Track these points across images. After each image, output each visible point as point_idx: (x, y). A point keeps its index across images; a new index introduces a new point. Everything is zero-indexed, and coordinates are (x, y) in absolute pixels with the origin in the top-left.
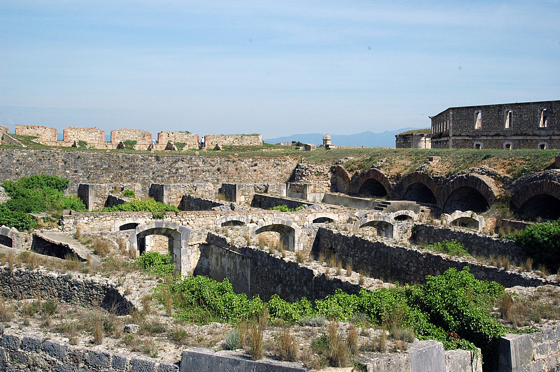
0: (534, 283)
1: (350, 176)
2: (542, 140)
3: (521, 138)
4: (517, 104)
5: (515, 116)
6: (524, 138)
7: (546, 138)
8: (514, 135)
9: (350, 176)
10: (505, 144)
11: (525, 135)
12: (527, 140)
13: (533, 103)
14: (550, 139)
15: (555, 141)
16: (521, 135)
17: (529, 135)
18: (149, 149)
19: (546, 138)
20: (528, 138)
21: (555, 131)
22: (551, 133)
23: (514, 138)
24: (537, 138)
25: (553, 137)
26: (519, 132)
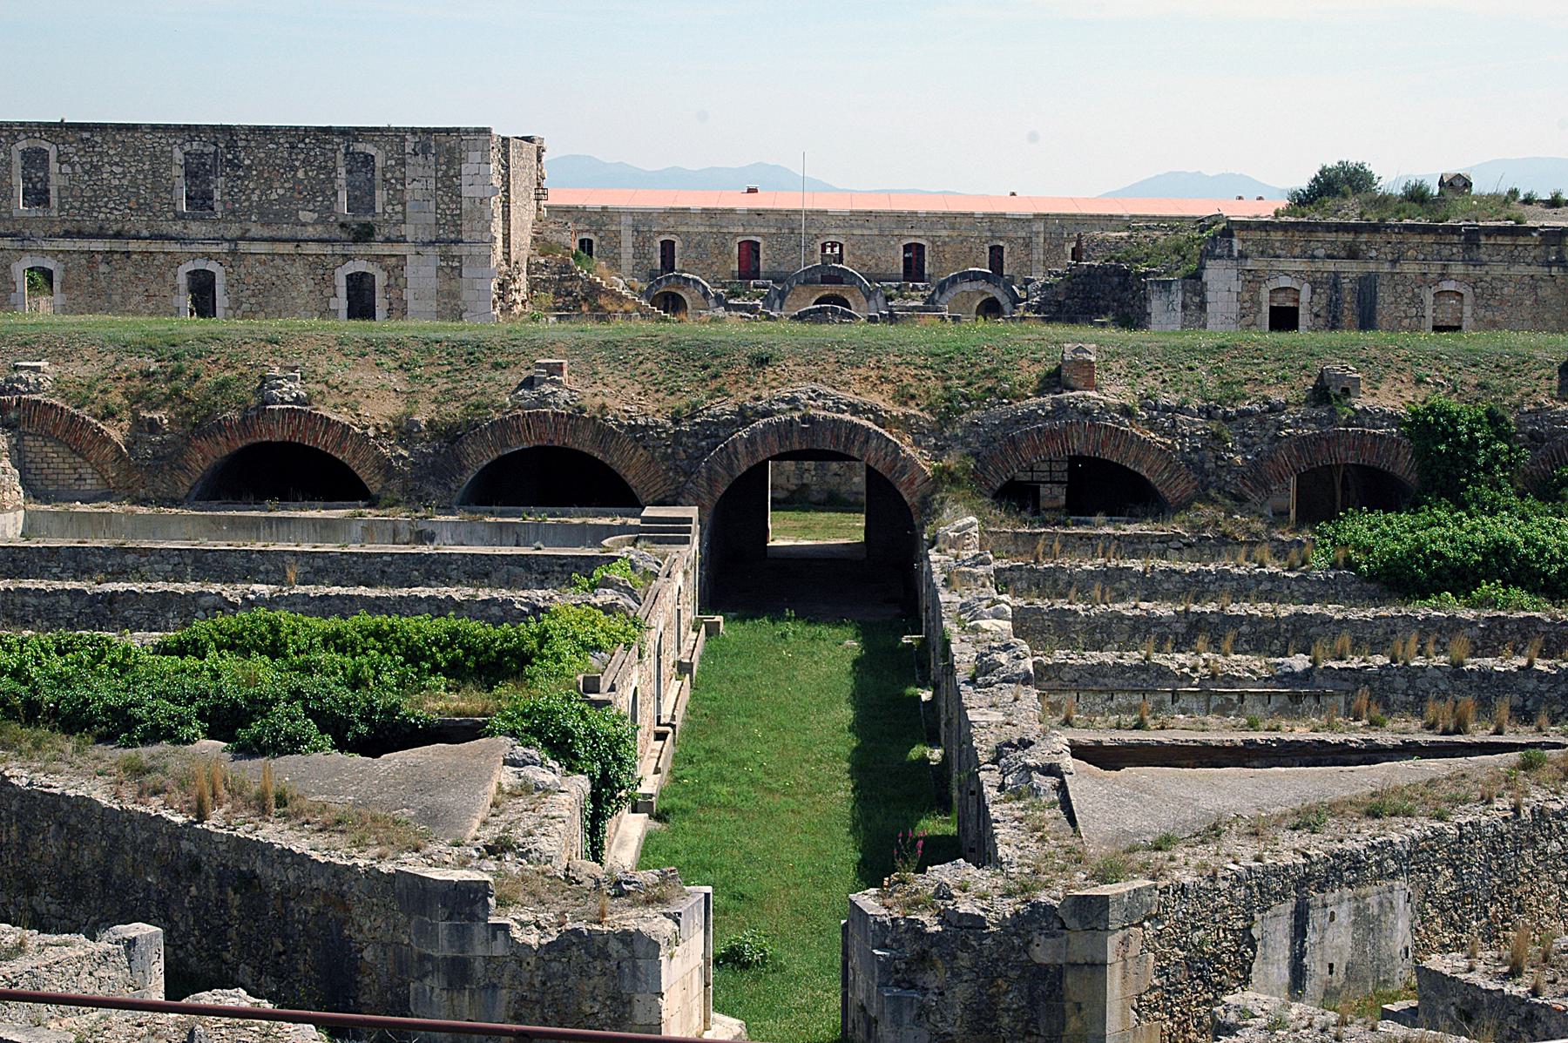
0: (854, 409)
1: (116, 433)
2: (194, 256)
3: (98, 245)
4: (61, 125)
5: (66, 169)
6: (117, 245)
7: (214, 249)
8: (67, 234)
9: (116, 433)
10: (19, 269)
11: (118, 235)
12: (128, 254)
13: (154, 127)
14: (233, 253)
15: (251, 260)
16: (100, 234)
17: (137, 238)
18: (945, 420)
19: (214, 249)
20: (133, 246)
21: (249, 225)
22: (234, 230)
23: (66, 244)
24: (174, 247)
25: (243, 246)
26: (89, 226)
